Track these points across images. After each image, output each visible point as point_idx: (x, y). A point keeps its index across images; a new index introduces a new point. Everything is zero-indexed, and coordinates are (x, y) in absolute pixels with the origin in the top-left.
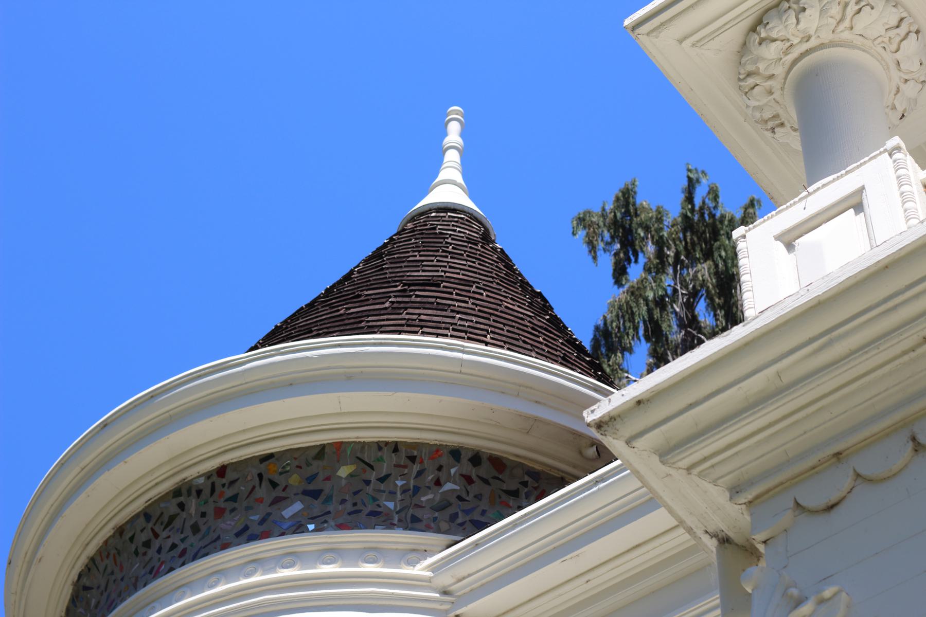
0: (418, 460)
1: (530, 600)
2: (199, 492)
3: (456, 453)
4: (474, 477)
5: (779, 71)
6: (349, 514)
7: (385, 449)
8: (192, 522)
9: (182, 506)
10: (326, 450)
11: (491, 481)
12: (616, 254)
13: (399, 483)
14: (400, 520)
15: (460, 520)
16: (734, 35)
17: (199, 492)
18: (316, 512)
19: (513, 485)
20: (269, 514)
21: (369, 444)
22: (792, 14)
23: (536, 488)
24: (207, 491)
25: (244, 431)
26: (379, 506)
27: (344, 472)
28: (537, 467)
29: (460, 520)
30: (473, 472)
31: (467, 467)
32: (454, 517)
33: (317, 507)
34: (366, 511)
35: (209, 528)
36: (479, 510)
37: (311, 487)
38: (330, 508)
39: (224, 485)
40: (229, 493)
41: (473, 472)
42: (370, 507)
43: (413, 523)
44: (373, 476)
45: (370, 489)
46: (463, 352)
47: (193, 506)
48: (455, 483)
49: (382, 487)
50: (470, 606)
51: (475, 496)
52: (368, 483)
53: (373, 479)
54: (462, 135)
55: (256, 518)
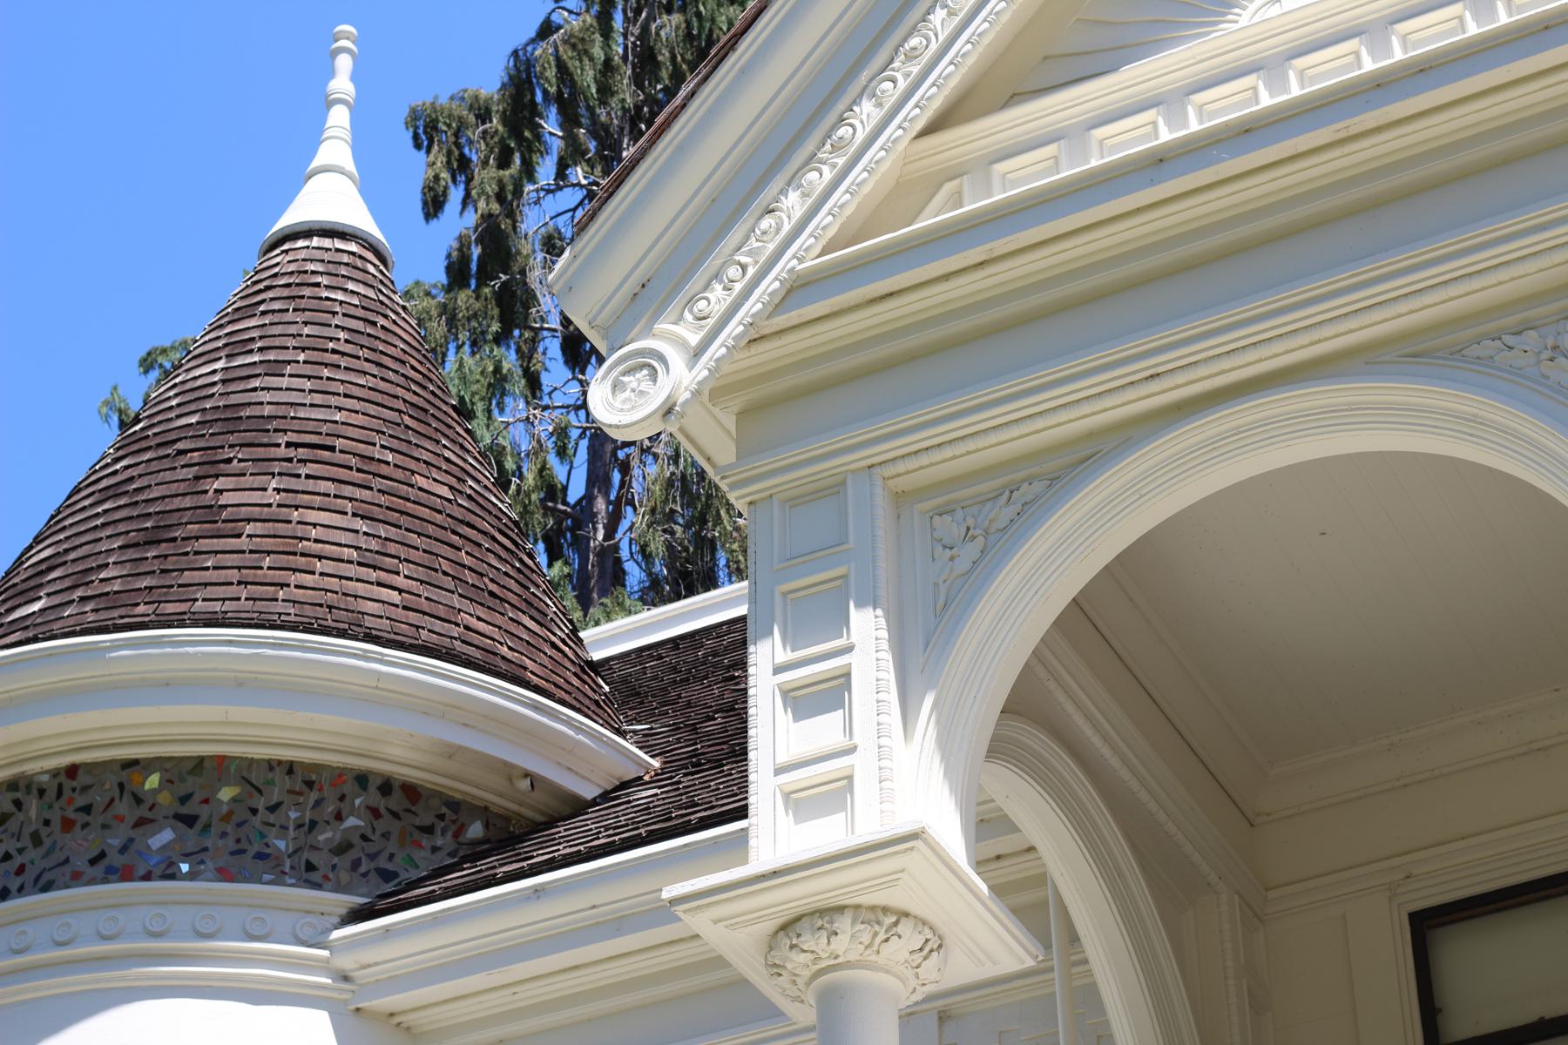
0: (316, 786)
1: (446, 1001)
2: (42, 792)
3: (362, 779)
4: (383, 811)
5: (806, 973)
6: (232, 854)
7: (277, 769)
8: (32, 828)
9: (18, 804)
10: (206, 764)
11: (402, 814)
13: (293, 815)
14: (292, 867)
15: (363, 869)
16: (770, 925)
17: (42, 792)
18: (191, 846)
19: (426, 819)
20: (131, 840)
21: (259, 761)
22: (824, 934)
23: (454, 822)
24: (51, 794)
25: (104, 729)
26: (267, 845)
28: (458, 796)
29: (363, 869)
30: (381, 803)
31: (375, 798)
32: (356, 864)
33: (192, 838)
34: (252, 850)
35: (55, 843)
36: (386, 854)
37: (184, 810)
38: (208, 843)
39: (74, 790)
40: (81, 801)
41: (381, 803)
42: (256, 847)
43: (308, 874)
45: (256, 821)
46: (381, 662)
47: (33, 808)
48: (359, 817)
49: (272, 818)
50: (374, 1002)
51: (383, 835)
52: (254, 811)
53: (261, 808)
54: (354, 78)
55: (116, 842)
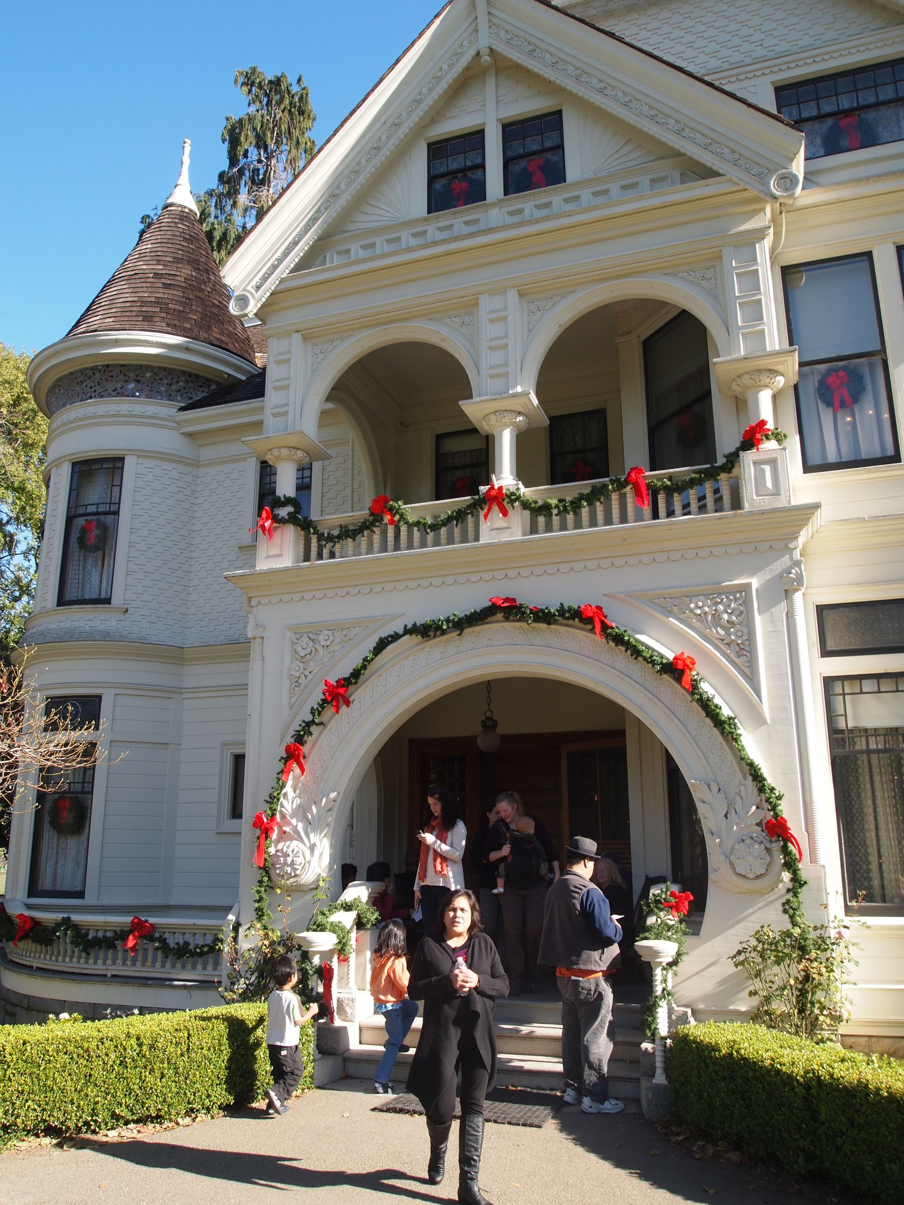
3: (184, 373)
12: (536, 502)
19: (201, 384)
27: (148, 375)
31: (187, 377)
33: (139, 386)
44: (157, 378)
